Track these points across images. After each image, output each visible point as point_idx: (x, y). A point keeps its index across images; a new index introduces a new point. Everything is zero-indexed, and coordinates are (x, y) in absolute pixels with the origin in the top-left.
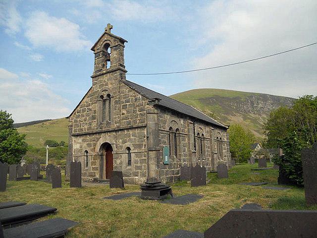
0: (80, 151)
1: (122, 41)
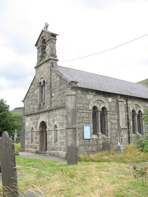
1: (54, 35)
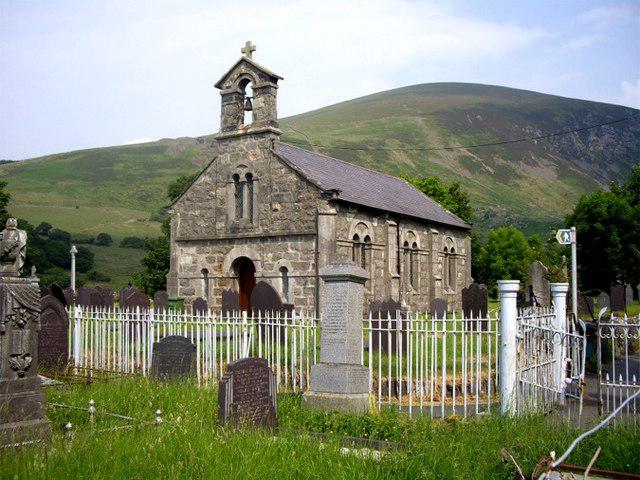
0: (193, 269)
1: (274, 79)
